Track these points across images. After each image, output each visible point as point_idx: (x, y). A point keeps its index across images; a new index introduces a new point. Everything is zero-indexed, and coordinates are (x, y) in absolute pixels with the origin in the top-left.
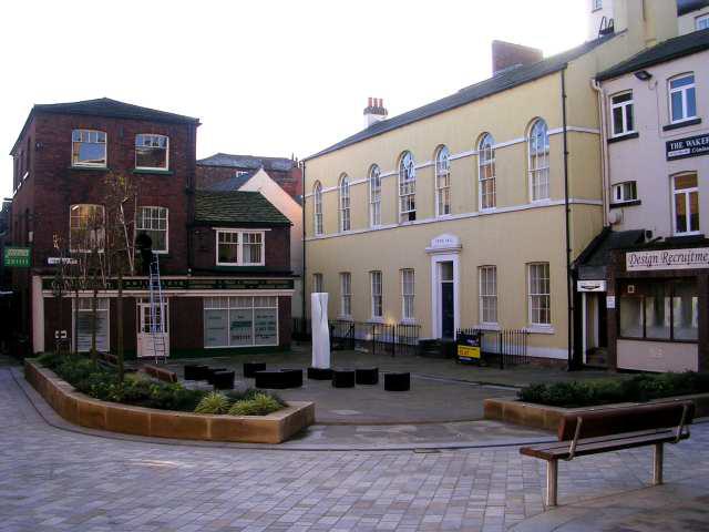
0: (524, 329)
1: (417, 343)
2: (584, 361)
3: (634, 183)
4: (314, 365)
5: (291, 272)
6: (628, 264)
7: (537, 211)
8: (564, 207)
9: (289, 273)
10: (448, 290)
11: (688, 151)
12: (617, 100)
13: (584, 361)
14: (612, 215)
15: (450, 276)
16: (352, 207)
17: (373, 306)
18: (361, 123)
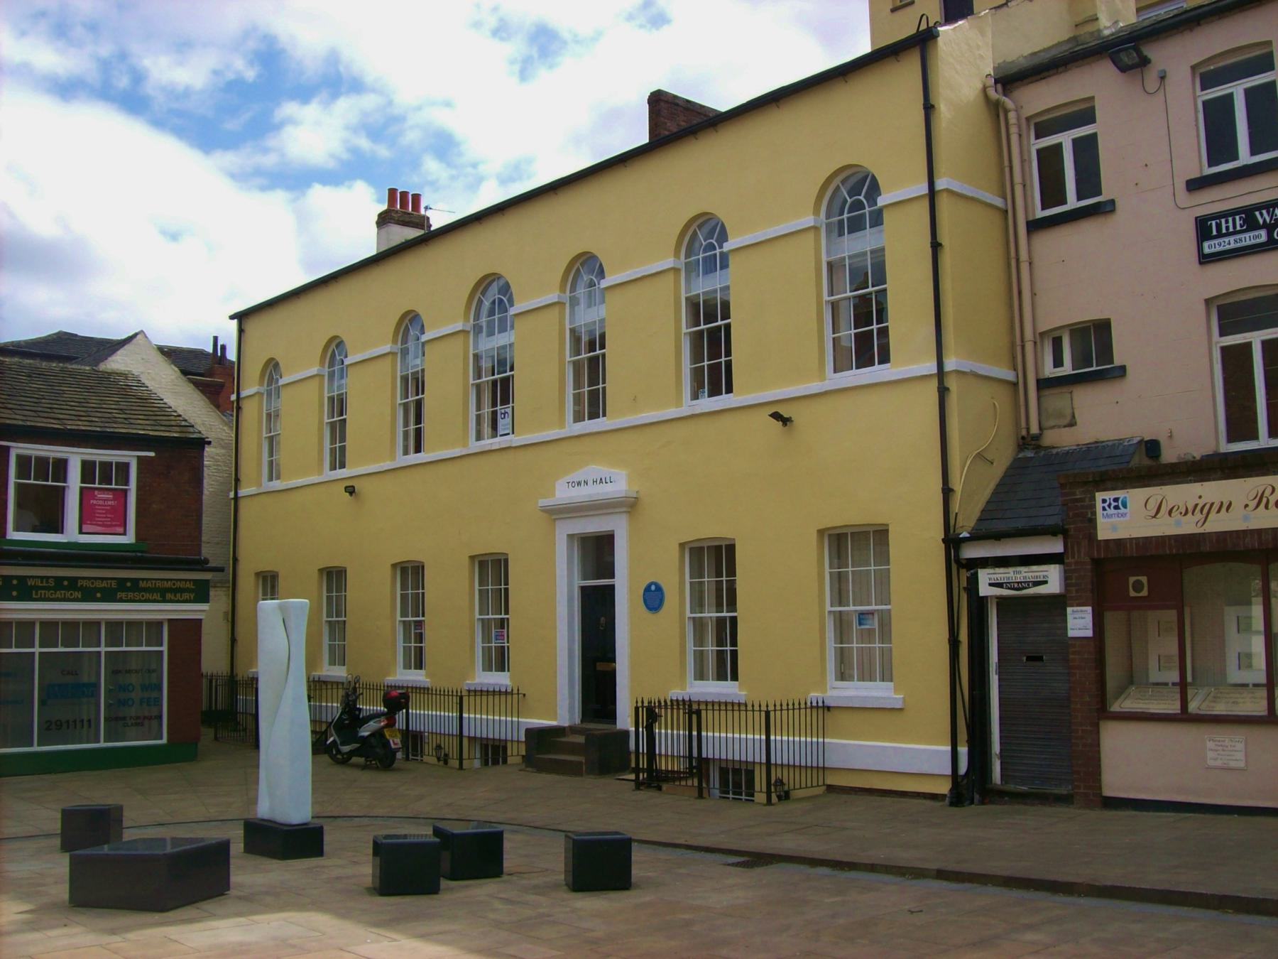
0: (815, 695)
3: (1103, 328)
4: (264, 809)
5: (206, 561)
8: (934, 384)
9: (201, 565)
10: (597, 609)
11: (1262, 236)
12: (1042, 130)
15: (607, 569)
16: (352, 416)
17: (400, 644)
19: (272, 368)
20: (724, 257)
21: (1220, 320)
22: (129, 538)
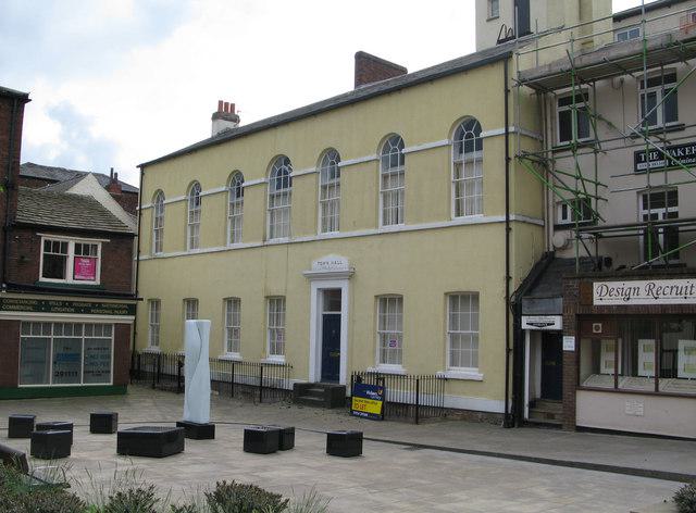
0: (440, 373)
1: (291, 388)
2: (526, 415)
6: (596, 296)
7: (463, 230)
10: (331, 328)
13: (526, 415)
14: (559, 238)
18: (204, 131)
19: (159, 195)
20: (403, 156)
21: (543, 361)
22: (98, 282)
